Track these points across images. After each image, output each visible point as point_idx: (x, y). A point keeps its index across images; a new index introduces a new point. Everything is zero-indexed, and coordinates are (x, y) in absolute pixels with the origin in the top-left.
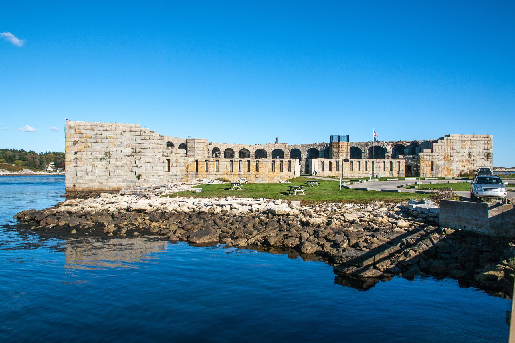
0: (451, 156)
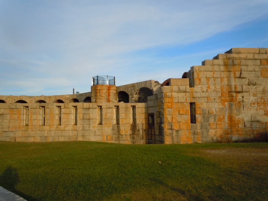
0: (239, 92)
